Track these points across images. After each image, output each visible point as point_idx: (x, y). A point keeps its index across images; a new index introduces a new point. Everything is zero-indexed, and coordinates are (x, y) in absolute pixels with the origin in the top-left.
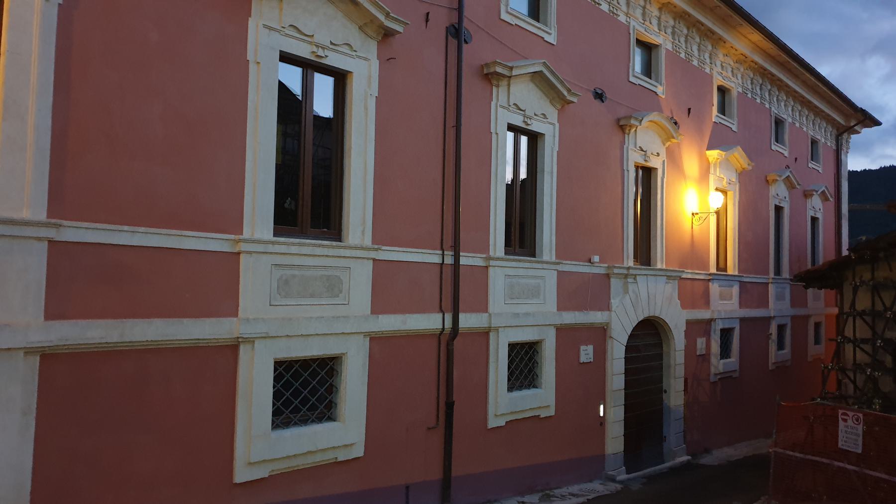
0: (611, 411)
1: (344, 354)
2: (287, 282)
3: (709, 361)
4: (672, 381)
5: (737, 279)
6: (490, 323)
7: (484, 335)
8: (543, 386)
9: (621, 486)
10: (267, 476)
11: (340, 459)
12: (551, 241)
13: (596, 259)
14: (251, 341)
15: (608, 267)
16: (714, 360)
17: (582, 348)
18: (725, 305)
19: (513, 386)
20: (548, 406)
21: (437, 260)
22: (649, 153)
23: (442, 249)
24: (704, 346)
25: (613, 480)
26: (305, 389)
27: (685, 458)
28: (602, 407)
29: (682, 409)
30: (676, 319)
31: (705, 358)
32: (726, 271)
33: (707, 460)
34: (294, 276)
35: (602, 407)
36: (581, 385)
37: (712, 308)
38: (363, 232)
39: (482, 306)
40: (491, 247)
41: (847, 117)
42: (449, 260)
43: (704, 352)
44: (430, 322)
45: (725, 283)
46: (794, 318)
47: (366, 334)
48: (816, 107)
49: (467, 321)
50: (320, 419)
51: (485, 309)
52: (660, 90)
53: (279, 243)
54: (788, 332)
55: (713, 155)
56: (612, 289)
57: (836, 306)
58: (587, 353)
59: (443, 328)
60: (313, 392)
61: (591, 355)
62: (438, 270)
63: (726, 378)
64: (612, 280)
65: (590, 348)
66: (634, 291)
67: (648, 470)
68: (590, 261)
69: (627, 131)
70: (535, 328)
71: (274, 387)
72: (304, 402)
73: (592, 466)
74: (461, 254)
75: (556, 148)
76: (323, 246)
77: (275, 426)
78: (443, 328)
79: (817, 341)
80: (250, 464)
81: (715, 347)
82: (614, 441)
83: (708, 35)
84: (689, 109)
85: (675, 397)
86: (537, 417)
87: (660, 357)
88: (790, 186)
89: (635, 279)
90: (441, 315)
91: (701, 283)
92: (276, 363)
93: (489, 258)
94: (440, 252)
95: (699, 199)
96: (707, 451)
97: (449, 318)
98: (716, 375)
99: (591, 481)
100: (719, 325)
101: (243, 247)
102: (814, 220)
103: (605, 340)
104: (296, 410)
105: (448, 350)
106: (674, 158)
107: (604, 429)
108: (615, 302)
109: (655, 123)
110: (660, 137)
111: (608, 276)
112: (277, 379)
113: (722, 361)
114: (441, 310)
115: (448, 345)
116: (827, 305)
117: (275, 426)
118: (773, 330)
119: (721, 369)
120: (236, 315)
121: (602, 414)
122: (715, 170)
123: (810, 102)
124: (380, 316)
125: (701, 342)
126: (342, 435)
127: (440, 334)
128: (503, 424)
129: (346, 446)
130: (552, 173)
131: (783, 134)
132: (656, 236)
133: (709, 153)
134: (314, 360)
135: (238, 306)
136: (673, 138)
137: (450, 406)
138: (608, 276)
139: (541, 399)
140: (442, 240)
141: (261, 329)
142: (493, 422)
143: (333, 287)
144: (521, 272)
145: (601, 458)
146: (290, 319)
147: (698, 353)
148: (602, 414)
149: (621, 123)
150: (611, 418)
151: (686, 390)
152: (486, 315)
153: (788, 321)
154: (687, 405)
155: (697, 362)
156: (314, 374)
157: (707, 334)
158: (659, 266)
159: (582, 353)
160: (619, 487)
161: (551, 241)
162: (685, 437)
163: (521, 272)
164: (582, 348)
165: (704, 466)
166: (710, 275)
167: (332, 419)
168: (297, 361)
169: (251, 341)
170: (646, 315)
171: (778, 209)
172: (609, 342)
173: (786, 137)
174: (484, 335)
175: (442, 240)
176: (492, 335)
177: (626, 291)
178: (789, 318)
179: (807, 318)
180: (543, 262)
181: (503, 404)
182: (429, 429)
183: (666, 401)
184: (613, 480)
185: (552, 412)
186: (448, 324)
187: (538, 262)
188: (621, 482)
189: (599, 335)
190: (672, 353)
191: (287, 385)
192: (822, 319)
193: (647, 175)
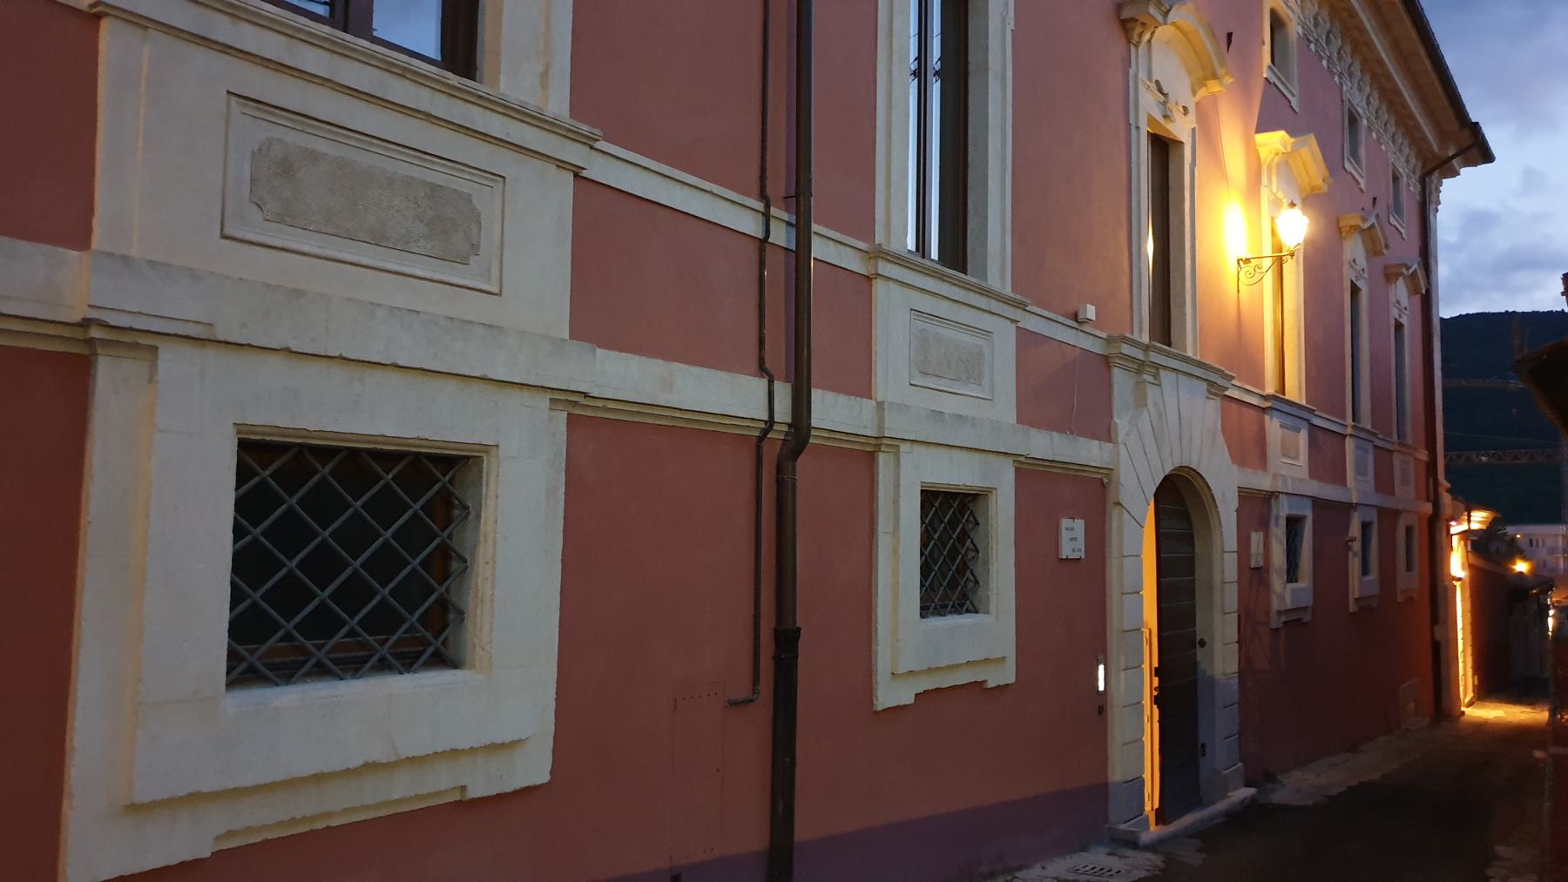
0: (1129, 681)
1: (486, 448)
2: (286, 168)
5: (1305, 415)
6: (881, 427)
7: (863, 456)
8: (993, 608)
10: (206, 854)
11: (475, 792)
12: (1003, 247)
13: (1091, 312)
14: (139, 343)
15: (1109, 341)
16: (1277, 582)
17: (1065, 523)
18: (1289, 466)
19: (932, 605)
21: (749, 224)
22: (1171, 105)
23: (763, 197)
25: (1132, 843)
26: (347, 551)
27: (1245, 792)
28: (1101, 668)
30: (1225, 482)
33: (1280, 796)
34: (315, 157)
35: (1101, 668)
36: (1067, 610)
38: (544, 77)
39: (859, 383)
40: (879, 228)
41: (1443, 137)
43: (1261, 564)
44: (736, 396)
45: (1290, 421)
47: (562, 398)
48: (1405, 106)
49: (832, 411)
50: (407, 661)
51: (866, 391)
55: (1274, 142)
58: (1072, 538)
59: (771, 422)
60: (385, 564)
61: (1081, 544)
62: (752, 251)
63: (1294, 622)
64: (1116, 372)
65: (1079, 525)
66: (1155, 404)
68: (1075, 317)
69: (1136, 38)
70: (977, 455)
71: (238, 532)
72: (353, 595)
73: (1086, 812)
74: (815, 227)
75: (1011, 26)
77: (242, 673)
78: (771, 422)
79: (1409, 568)
80: (134, 808)
81: (1279, 557)
84: (1230, 35)
85: (1222, 659)
86: (979, 685)
88: (1373, 251)
89: (1156, 376)
90: (764, 382)
92: (245, 446)
93: (878, 254)
94: (760, 206)
95: (1253, 229)
97: (783, 392)
98: (1279, 613)
99: (1084, 849)
100: (1283, 509)
103: (1104, 512)
104: (321, 625)
105: (780, 483)
106: (1207, 129)
107: (1105, 721)
108: (1121, 423)
109: (1184, 33)
110: (1189, 72)
112: (249, 507)
113: (1290, 586)
114: (763, 370)
115: (779, 469)
117: (242, 673)
118: (1355, 530)
119: (1289, 603)
120: (79, 237)
121: (1101, 688)
122: (1270, 180)
123: (1398, 93)
124: (600, 352)
126: (489, 707)
127: (761, 439)
128: (909, 699)
129: (494, 748)
130: (1004, 77)
133: (1261, 138)
134: (387, 457)
135: (89, 211)
136: (1215, 76)
137: (787, 639)
138: (1106, 360)
139: (984, 642)
140: (763, 170)
141: (182, 305)
142: (891, 694)
143: (449, 229)
144: (944, 309)
146: (298, 293)
147: (1253, 565)
148: (1101, 688)
149: (1126, 14)
152: (869, 405)
153: (1373, 516)
156: (386, 507)
157: (1264, 525)
158: (1190, 354)
159: (1065, 536)
160: (1156, 860)
161: (1003, 247)
163: (944, 309)
164: (1065, 523)
165: (1284, 809)
166: (1266, 398)
167: (444, 659)
168: (325, 453)
169: (139, 343)
170: (1168, 469)
171: (1355, 291)
172: (1115, 513)
173: (1362, 152)
174: (863, 456)
175: (763, 170)
176: (884, 461)
177: (1141, 402)
181: (913, 648)
182: (734, 704)
184: (1132, 843)
185: (534, 768)
186: (783, 412)
187: (966, 286)
188: (1152, 847)
189: (1093, 493)
191: (290, 534)
193: (1163, 148)
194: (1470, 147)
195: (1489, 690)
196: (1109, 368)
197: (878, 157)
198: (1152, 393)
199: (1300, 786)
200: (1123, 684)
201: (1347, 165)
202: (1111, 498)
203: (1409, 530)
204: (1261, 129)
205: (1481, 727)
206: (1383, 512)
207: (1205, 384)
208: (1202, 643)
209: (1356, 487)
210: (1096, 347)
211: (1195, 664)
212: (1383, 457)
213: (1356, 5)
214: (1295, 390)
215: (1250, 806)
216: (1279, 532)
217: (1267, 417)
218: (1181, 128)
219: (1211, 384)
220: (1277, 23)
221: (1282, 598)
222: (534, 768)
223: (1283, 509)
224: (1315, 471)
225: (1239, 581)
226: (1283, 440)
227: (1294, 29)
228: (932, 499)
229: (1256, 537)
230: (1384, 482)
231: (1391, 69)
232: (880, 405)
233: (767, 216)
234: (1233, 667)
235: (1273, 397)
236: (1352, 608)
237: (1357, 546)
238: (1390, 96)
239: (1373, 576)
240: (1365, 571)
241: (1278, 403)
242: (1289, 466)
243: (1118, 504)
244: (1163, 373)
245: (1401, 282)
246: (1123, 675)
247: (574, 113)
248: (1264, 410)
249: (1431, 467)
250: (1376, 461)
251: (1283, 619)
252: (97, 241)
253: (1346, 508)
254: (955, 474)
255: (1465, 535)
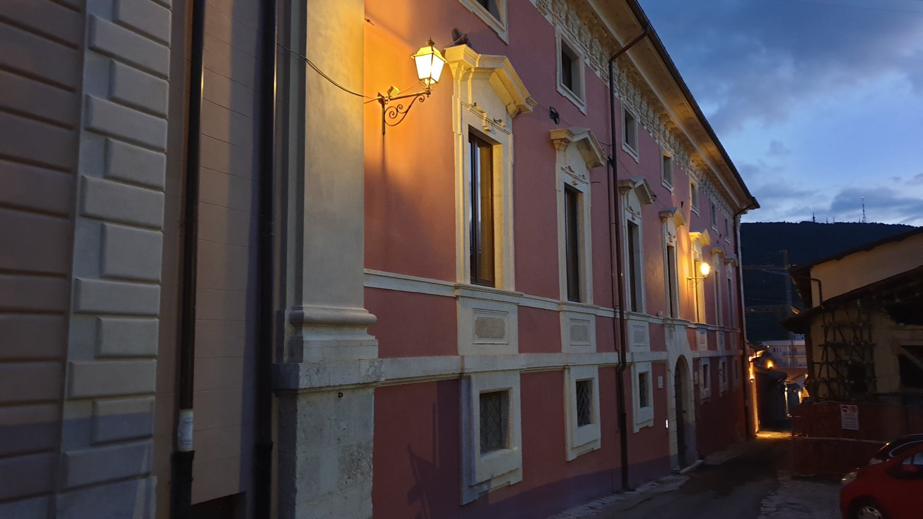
16: (702, 389)
20: (517, 469)
21: (611, 315)
27: (700, 461)
30: (689, 357)
32: (493, 285)
41: (741, 201)
42: (618, 316)
46: (528, 377)
51: (457, 354)
52: (672, 190)
53: (570, 305)
54: (709, 369)
55: (695, 235)
57: (616, 350)
76: (479, 290)
79: (643, 403)
81: (702, 381)
83: (653, 102)
100: (702, 363)
101: (675, 322)
102: (631, 226)
116: (600, 349)
123: (726, 192)
131: (633, 132)
133: (691, 234)
138: (663, 325)
142: (571, 456)
153: (726, 361)
158: (679, 318)
173: (673, 175)
177: (671, 337)
178: (596, 369)
179: (558, 374)
180: (641, 316)
185: (598, 446)
187: (638, 315)
192: (592, 374)
193: (670, 248)
194: (642, 37)
195: (764, 427)
198: (674, 333)
199: (714, 459)
201: (624, 148)
203: (642, 376)
204: (691, 231)
205: (764, 440)
206: (711, 359)
209: (720, 350)
210: (660, 322)
212: (711, 335)
213: (592, 4)
214: (703, 321)
216: (702, 371)
218: (673, 244)
220: (693, 186)
222: (598, 446)
223: (702, 363)
224: (710, 348)
227: (697, 187)
228: (484, 396)
229: (696, 374)
230: (728, 347)
231: (653, 88)
232: (463, 357)
233: (615, 312)
234: (694, 419)
236: (721, 395)
237: (721, 372)
238: (724, 194)
239: (726, 383)
240: (724, 381)
241: (699, 325)
242: (703, 348)
245: (730, 265)
247: (595, 303)
249: (742, 334)
250: (708, 336)
252: (563, 350)
253: (718, 358)
254: (584, 376)
255: (753, 360)
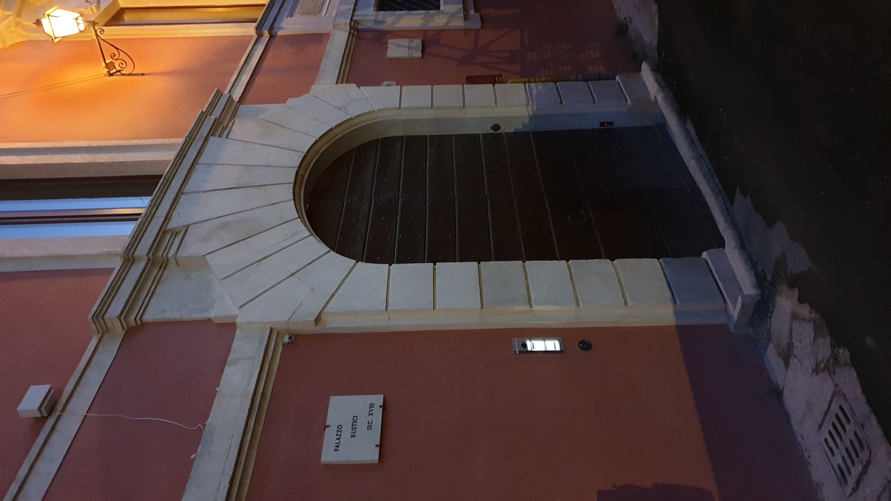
3: (440, 31)
4: (470, 113)
9: (738, 196)
16: (438, 21)
24: (405, 42)
28: (537, 345)
29: (536, 88)
30: (330, 105)
31: (430, 41)
35: (537, 345)
37: (328, 28)
43: (417, 42)
56: (177, 315)
64: (149, 317)
66: (206, 239)
67: (692, 165)
68: (39, 422)
80: (482, 308)
82: (625, 293)
85: (506, 105)
87: (441, 141)
91: (271, 53)
96: (622, 30)
98: (466, 18)
111: (135, 332)
121: (553, 345)
125: (396, 49)
132: (112, 165)
145: (693, 340)
148: (553, 345)
150: (561, 313)
151: (493, 80)
154: (527, 75)
155: (437, 60)
157: (381, 37)
162: (599, 78)
166: (260, 36)
183: (520, 127)
190: (405, 115)
196: (143, 325)
197: (85, 356)
200: (548, 308)
202: (311, 329)
207: (212, 139)
208: (496, 127)
211: (517, 134)
215: (667, 73)
217: (280, 33)
219: (212, 132)
221: (452, 15)
225: (432, 82)
226: (307, 13)
229: (396, 49)
235: (259, 29)
243: (318, 320)
244: (174, 224)
246: (536, 308)
248: (272, 36)
251: (472, 12)
